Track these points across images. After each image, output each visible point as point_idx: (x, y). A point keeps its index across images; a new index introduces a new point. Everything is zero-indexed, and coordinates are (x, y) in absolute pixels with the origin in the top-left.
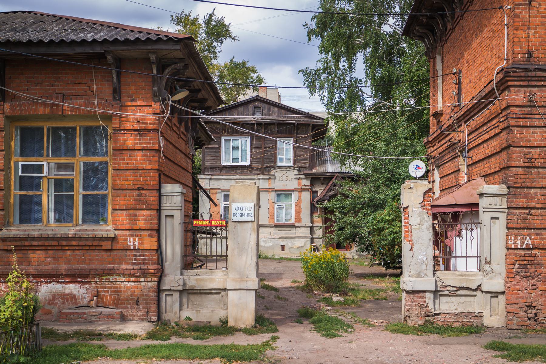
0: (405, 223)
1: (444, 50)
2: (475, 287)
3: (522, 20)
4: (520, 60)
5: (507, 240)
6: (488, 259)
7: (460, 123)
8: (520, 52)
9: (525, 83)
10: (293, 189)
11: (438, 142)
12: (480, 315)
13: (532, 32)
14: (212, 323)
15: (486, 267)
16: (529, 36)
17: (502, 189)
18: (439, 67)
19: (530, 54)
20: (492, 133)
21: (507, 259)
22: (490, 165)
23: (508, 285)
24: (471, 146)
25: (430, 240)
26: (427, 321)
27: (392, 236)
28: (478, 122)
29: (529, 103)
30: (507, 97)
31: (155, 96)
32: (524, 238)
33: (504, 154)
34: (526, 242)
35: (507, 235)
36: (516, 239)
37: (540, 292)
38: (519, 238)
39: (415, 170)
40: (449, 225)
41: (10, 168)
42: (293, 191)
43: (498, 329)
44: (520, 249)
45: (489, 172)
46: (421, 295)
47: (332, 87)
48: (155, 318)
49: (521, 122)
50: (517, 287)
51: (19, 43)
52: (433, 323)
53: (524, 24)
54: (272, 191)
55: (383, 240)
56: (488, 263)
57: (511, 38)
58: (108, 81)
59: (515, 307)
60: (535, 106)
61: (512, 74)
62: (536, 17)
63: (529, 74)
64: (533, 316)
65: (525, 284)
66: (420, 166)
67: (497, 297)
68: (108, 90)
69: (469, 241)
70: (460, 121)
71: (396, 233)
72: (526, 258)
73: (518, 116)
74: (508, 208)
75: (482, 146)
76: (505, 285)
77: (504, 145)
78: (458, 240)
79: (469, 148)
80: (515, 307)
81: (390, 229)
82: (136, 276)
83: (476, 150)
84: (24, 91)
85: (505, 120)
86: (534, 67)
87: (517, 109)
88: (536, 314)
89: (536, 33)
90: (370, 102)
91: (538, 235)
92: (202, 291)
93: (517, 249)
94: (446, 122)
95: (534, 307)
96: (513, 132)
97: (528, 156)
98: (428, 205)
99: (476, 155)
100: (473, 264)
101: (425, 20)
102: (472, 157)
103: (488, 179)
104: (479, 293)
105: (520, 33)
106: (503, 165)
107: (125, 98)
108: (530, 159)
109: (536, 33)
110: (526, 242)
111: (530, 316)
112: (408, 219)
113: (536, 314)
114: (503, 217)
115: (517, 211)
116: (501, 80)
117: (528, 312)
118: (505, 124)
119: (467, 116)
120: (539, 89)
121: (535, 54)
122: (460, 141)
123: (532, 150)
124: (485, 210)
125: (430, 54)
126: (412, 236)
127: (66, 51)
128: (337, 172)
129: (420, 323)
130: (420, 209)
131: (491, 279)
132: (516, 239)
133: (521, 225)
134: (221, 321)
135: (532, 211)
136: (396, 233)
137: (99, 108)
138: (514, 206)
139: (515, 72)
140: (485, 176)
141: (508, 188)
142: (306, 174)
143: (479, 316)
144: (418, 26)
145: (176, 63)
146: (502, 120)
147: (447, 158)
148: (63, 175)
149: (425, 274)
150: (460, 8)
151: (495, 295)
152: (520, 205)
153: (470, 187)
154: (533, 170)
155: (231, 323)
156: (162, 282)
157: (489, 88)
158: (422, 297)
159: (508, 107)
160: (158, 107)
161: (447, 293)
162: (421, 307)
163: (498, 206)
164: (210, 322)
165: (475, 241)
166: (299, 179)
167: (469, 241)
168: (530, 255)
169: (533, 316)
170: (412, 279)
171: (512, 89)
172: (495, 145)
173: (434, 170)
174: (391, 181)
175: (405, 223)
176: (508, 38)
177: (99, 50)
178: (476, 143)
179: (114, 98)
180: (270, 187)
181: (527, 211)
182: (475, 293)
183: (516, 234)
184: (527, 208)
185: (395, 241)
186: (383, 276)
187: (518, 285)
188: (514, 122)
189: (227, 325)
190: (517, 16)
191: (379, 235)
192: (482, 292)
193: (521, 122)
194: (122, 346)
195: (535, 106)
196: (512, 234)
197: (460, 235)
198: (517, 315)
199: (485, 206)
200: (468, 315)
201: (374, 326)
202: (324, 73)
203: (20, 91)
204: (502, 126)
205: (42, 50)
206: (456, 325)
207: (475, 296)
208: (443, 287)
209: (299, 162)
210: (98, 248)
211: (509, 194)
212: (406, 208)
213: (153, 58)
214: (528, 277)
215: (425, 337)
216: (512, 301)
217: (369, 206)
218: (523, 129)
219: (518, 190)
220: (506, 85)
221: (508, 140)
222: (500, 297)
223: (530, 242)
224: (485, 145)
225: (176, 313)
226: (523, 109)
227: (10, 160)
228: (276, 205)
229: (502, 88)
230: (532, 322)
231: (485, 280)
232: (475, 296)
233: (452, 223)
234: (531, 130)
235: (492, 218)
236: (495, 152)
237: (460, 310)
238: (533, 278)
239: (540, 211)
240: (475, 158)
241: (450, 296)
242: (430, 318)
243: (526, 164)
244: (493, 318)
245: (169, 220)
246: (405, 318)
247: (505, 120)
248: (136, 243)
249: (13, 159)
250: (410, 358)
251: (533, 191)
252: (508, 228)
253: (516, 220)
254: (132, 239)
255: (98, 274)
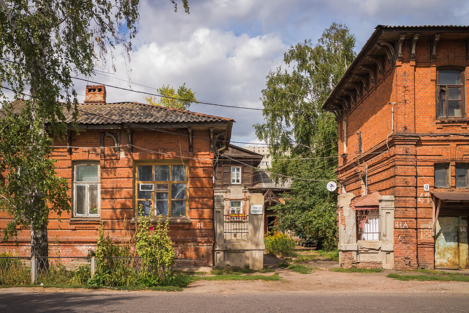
0: (341, 215)
1: (349, 119)
2: (378, 248)
3: (401, 110)
4: (400, 131)
5: (395, 224)
6: (385, 234)
7: (362, 162)
8: (400, 127)
9: (404, 143)
10: (241, 198)
11: (345, 172)
12: (380, 263)
13: (406, 116)
14: (241, 267)
15: (384, 238)
16: (405, 119)
17: (392, 197)
18: (344, 128)
19: (406, 128)
20: (385, 168)
21: (394, 234)
22: (383, 185)
23: (395, 247)
24: (370, 174)
25: (354, 224)
26: (353, 266)
27: (317, 225)
28: (375, 162)
29: (405, 153)
30: (392, 151)
31: (210, 149)
32: (403, 223)
33: (392, 180)
34: (405, 225)
35: (395, 221)
36: (399, 223)
37: (412, 251)
38: (401, 223)
39: (330, 187)
40: (363, 216)
41: (135, 187)
42: (241, 200)
43: (390, 270)
44: (402, 229)
45: (382, 188)
46: (350, 252)
47: (273, 135)
48: (212, 265)
49: (401, 163)
50: (400, 248)
51: (145, 123)
52: (356, 267)
53: (402, 112)
54: (228, 200)
55: (312, 227)
56: (385, 236)
57: (396, 119)
58: (186, 142)
59: (399, 259)
60: (409, 155)
61: (397, 138)
62: (409, 108)
63: (406, 138)
64: (408, 263)
65: (404, 246)
66: (333, 185)
67: (389, 253)
68: (186, 146)
69: (374, 225)
70: (362, 160)
71: (320, 224)
72: (405, 233)
73: (400, 160)
74: (395, 207)
75: (377, 175)
76: (394, 247)
77: (392, 175)
78: (366, 224)
79: (369, 175)
80: (399, 259)
81: (316, 222)
82: (202, 243)
83: (373, 177)
84: (143, 147)
85: (393, 162)
86: (408, 135)
87: (400, 156)
88: (410, 262)
89: (409, 117)
90: (295, 145)
91: (410, 221)
92: (235, 251)
93: (400, 229)
94: (350, 160)
95: (409, 258)
96: (397, 168)
97: (405, 181)
98: (353, 206)
99: (373, 180)
100: (376, 236)
101: (337, 102)
102: (370, 181)
103: (382, 192)
104: (380, 252)
105: (400, 117)
106: (392, 185)
107: (195, 151)
108: (407, 182)
109: (409, 117)
110: (405, 225)
111: (407, 263)
112: (343, 213)
113: (410, 262)
114: (392, 212)
115: (400, 209)
116: (391, 141)
117: (406, 261)
118: (393, 164)
119: (367, 158)
120: (410, 146)
121: (408, 128)
122: (361, 171)
123: (407, 177)
124: (383, 208)
125: (339, 120)
126: (345, 222)
127: (169, 127)
128: (269, 188)
129: (349, 267)
130: (349, 208)
131: (386, 244)
132: (399, 223)
133: (402, 216)
134: (245, 266)
135: (407, 209)
136: (320, 224)
137: (182, 156)
138: (398, 206)
139: (398, 137)
140: (379, 191)
141: (395, 197)
142: (249, 190)
143: (380, 263)
144: (332, 104)
145: (221, 132)
146: (391, 161)
147: (352, 180)
148: (162, 190)
149: (352, 242)
150: (361, 98)
151: (388, 252)
152: (401, 206)
153: (372, 197)
154: (408, 188)
155: (251, 268)
156: (215, 246)
157: (382, 144)
158: (350, 254)
159: (394, 155)
160: (213, 155)
161: (363, 251)
162: (350, 259)
163: (390, 207)
164: (240, 267)
165: (377, 225)
166: (245, 192)
167: (374, 225)
168: (407, 232)
169: (408, 263)
170: (345, 245)
171: (396, 146)
172: (385, 175)
173: (342, 187)
174: (312, 194)
175: (341, 215)
176: (394, 119)
177: (185, 126)
178: (373, 173)
179: (190, 151)
180: (227, 198)
181: (405, 209)
182: (378, 252)
183: (399, 221)
184: (405, 208)
185: (319, 228)
186: (304, 250)
187: (400, 247)
188: (398, 163)
189: (249, 268)
190: (399, 108)
191: (310, 225)
192: (382, 251)
193: (401, 163)
194: (201, 276)
195: (409, 155)
196: (397, 221)
197: (367, 222)
198: (400, 263)
199: (383, 207)
200: (374, 263)
201: (322, 270)
202: (268, 127)
203: (141, 147)
204: (391, 165)
205: (156, 126)
206: (368, 268)
207: (378, 253)
208: (361, 248)
209: (245, 182)
210: (182, 228)
211: (395, 200)
212: (342, 207)
213: (212, 130)
214: (405, 243)
215: (354, 273)
216: (397, 255)
217: (300, 209)
218: (403, 167)
219: (400, 198)
220: (393, 144)
221: (394, 172)
222: (391, 253)
223: (406, 225)
224: (379, 174)
225: (222, 262)
226: (402, 156)
227: (135, 182)
228: (231, 209)
229: (391, 145)
230: (408, 266)
231: (383, 245)
232: (378, 253)
233: (365, 215)
234: (407, 167)
235: (387, 213)
236: (386, 178)
237: (370, 260)
238: (408, 244)
239: (411, 209)
240: (372, 181)
241: (365, 253)
242: (355, 265)
243: (404, 185)
244: (387, 264)
245: (218, 213)
246: (341, 265)
247: (393, 162)
248: (202, 226)
249: (136, 182)
250: (351, 281)
251: (408, 199)
252: (395, 218)
253: (399, 214)
254: (199, 224)
255: (182, 242)
